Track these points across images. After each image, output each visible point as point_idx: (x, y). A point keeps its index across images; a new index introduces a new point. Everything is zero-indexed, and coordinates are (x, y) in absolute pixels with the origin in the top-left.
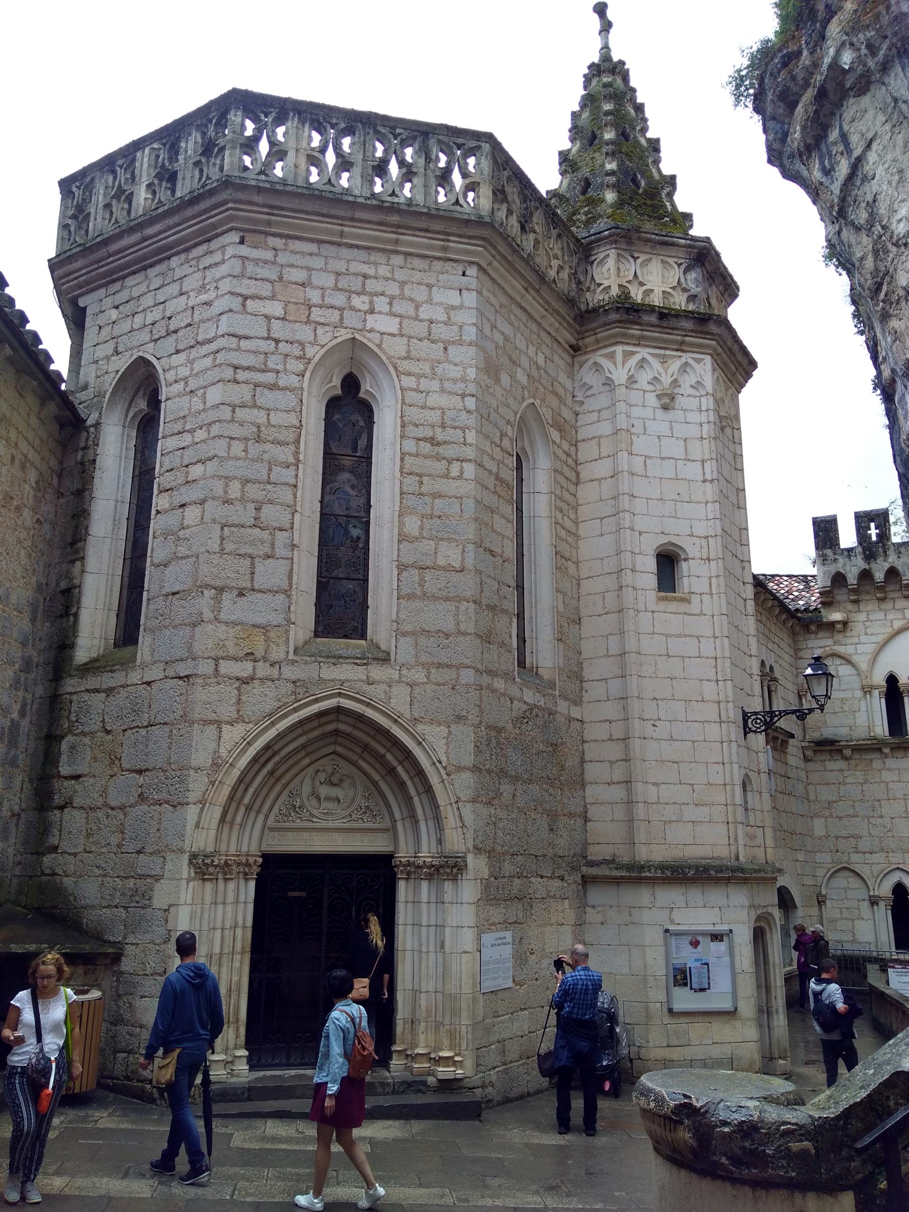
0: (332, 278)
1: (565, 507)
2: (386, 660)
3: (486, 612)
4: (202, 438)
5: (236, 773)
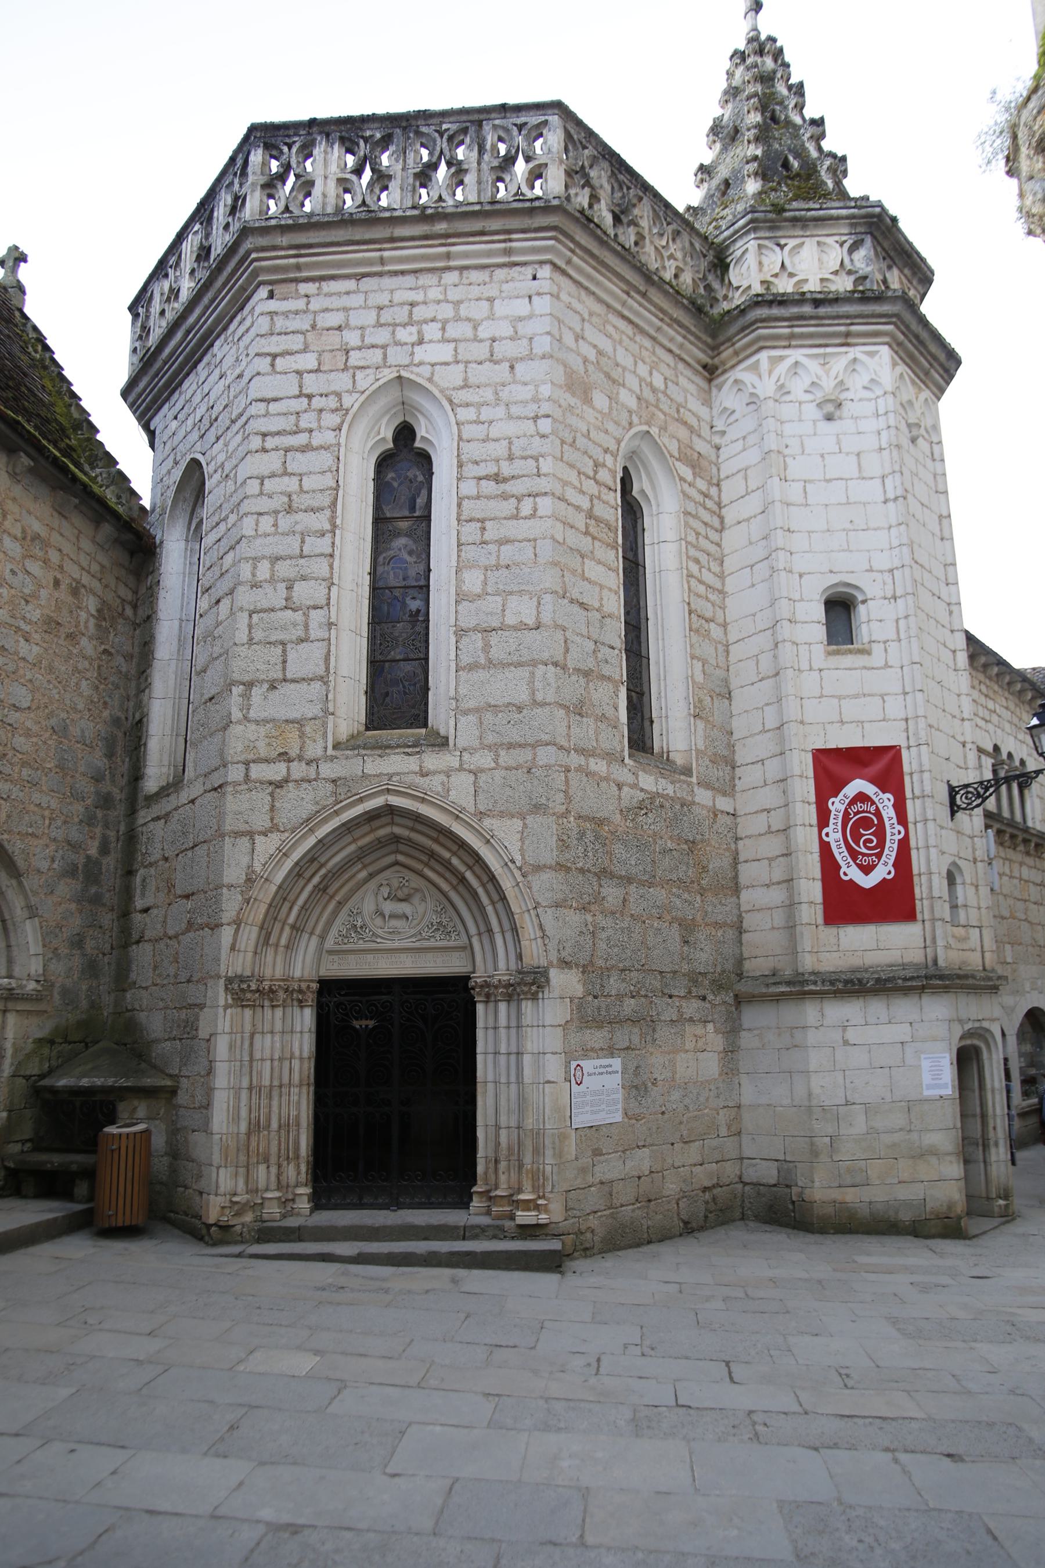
1: (703, 558)
2: (443, 745)
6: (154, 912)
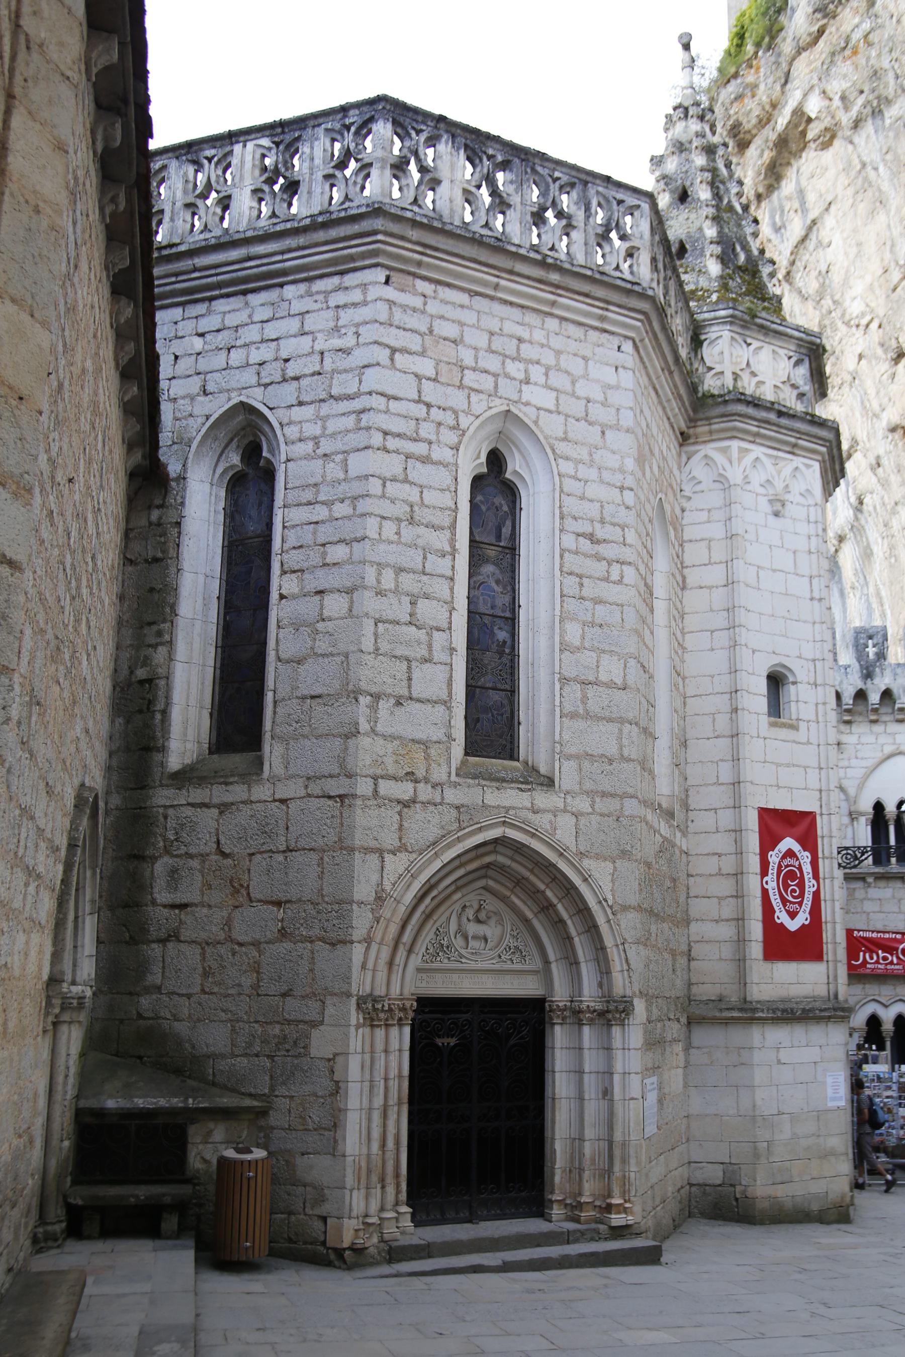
0: (486, 336)
4: (345, 513)
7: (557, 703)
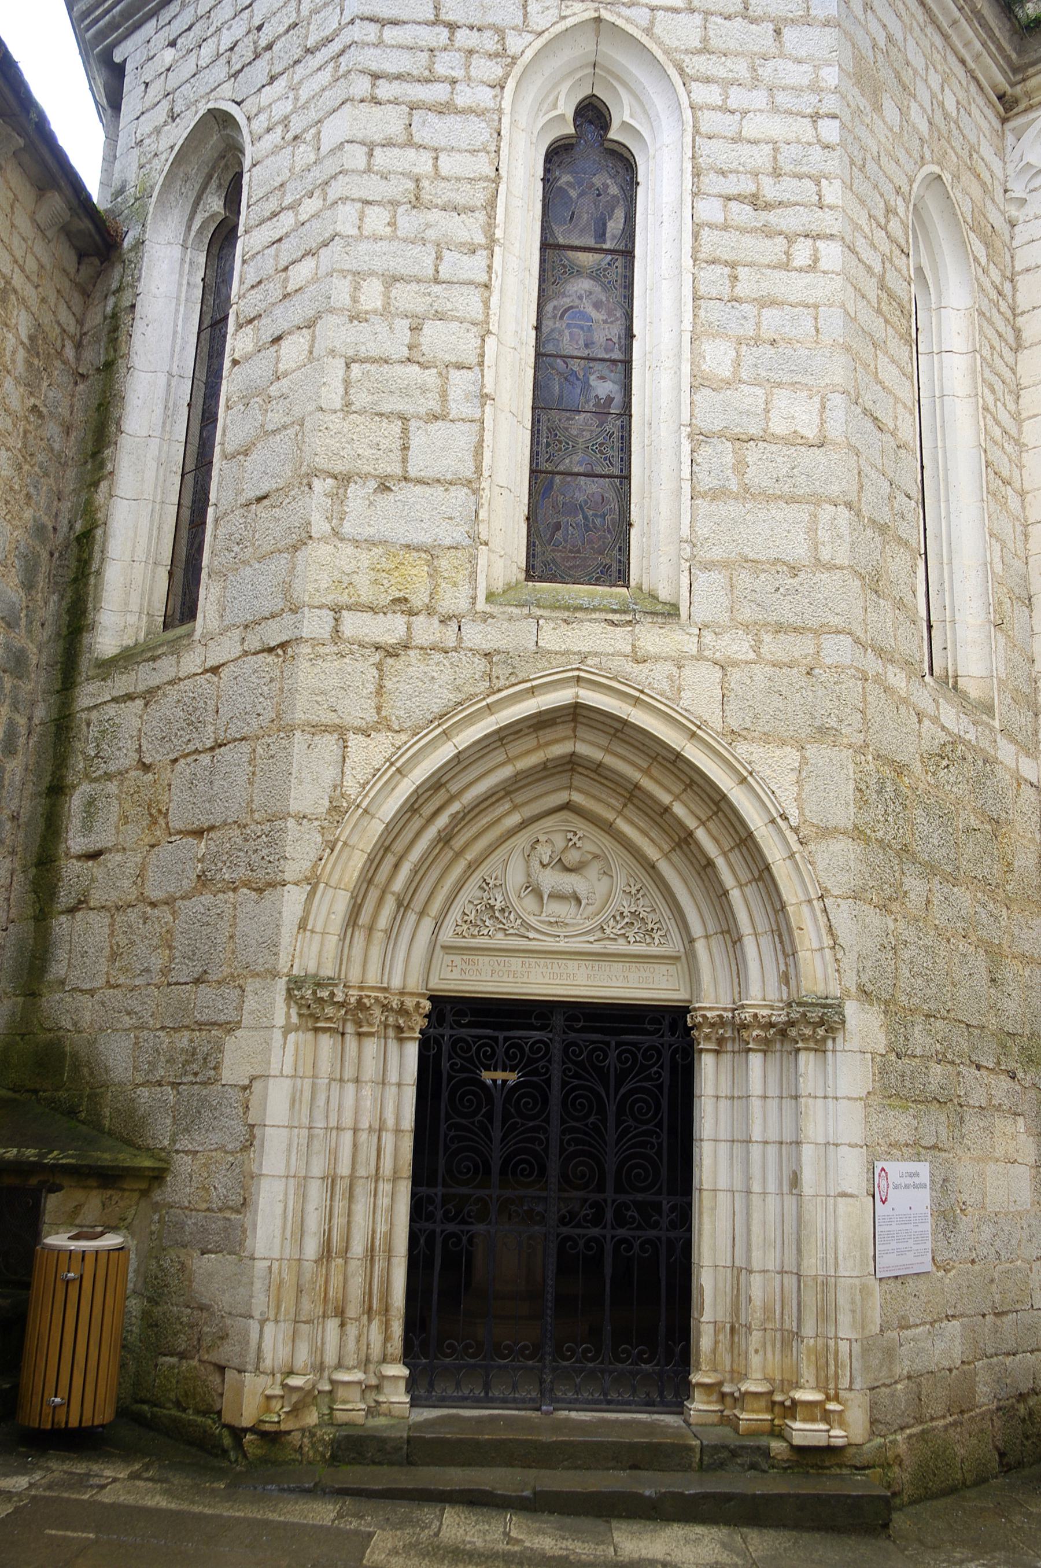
1: (999, 386)
3: (869, 532)
5: (377, 827)
6: (114, 859)
7: (686, 473)
